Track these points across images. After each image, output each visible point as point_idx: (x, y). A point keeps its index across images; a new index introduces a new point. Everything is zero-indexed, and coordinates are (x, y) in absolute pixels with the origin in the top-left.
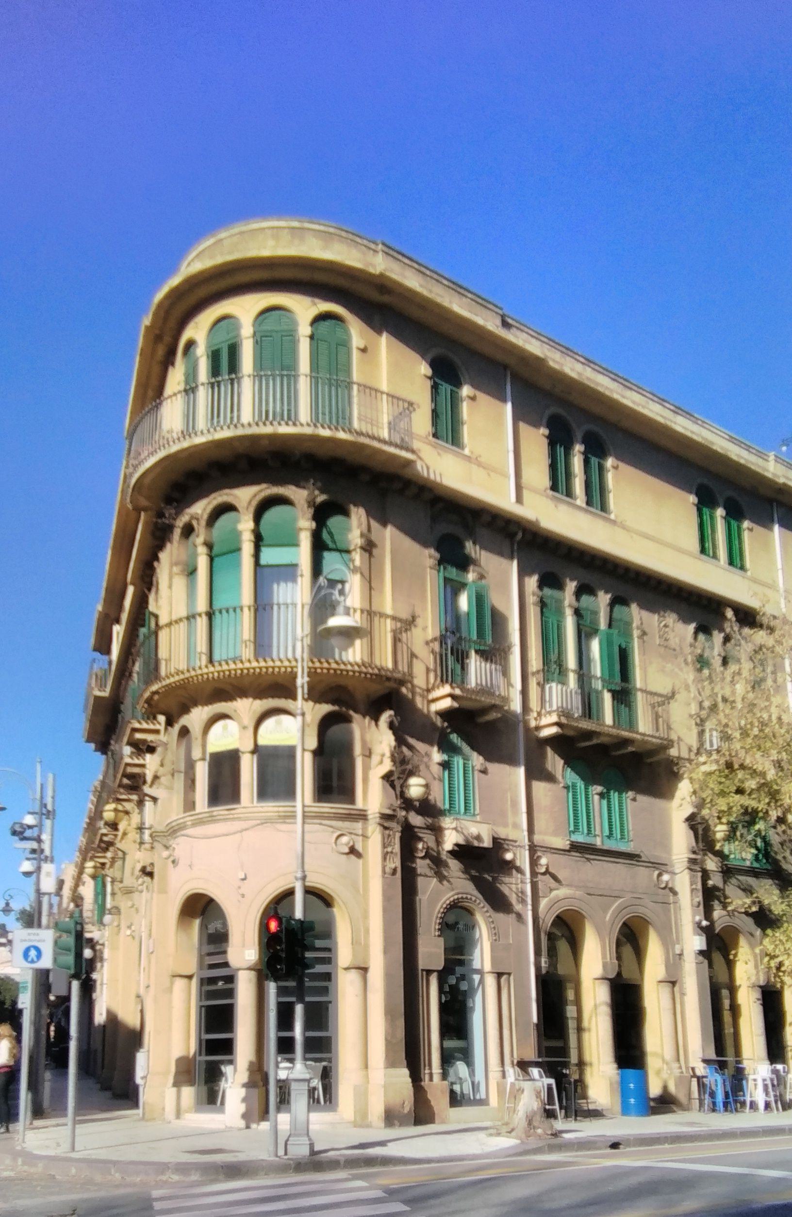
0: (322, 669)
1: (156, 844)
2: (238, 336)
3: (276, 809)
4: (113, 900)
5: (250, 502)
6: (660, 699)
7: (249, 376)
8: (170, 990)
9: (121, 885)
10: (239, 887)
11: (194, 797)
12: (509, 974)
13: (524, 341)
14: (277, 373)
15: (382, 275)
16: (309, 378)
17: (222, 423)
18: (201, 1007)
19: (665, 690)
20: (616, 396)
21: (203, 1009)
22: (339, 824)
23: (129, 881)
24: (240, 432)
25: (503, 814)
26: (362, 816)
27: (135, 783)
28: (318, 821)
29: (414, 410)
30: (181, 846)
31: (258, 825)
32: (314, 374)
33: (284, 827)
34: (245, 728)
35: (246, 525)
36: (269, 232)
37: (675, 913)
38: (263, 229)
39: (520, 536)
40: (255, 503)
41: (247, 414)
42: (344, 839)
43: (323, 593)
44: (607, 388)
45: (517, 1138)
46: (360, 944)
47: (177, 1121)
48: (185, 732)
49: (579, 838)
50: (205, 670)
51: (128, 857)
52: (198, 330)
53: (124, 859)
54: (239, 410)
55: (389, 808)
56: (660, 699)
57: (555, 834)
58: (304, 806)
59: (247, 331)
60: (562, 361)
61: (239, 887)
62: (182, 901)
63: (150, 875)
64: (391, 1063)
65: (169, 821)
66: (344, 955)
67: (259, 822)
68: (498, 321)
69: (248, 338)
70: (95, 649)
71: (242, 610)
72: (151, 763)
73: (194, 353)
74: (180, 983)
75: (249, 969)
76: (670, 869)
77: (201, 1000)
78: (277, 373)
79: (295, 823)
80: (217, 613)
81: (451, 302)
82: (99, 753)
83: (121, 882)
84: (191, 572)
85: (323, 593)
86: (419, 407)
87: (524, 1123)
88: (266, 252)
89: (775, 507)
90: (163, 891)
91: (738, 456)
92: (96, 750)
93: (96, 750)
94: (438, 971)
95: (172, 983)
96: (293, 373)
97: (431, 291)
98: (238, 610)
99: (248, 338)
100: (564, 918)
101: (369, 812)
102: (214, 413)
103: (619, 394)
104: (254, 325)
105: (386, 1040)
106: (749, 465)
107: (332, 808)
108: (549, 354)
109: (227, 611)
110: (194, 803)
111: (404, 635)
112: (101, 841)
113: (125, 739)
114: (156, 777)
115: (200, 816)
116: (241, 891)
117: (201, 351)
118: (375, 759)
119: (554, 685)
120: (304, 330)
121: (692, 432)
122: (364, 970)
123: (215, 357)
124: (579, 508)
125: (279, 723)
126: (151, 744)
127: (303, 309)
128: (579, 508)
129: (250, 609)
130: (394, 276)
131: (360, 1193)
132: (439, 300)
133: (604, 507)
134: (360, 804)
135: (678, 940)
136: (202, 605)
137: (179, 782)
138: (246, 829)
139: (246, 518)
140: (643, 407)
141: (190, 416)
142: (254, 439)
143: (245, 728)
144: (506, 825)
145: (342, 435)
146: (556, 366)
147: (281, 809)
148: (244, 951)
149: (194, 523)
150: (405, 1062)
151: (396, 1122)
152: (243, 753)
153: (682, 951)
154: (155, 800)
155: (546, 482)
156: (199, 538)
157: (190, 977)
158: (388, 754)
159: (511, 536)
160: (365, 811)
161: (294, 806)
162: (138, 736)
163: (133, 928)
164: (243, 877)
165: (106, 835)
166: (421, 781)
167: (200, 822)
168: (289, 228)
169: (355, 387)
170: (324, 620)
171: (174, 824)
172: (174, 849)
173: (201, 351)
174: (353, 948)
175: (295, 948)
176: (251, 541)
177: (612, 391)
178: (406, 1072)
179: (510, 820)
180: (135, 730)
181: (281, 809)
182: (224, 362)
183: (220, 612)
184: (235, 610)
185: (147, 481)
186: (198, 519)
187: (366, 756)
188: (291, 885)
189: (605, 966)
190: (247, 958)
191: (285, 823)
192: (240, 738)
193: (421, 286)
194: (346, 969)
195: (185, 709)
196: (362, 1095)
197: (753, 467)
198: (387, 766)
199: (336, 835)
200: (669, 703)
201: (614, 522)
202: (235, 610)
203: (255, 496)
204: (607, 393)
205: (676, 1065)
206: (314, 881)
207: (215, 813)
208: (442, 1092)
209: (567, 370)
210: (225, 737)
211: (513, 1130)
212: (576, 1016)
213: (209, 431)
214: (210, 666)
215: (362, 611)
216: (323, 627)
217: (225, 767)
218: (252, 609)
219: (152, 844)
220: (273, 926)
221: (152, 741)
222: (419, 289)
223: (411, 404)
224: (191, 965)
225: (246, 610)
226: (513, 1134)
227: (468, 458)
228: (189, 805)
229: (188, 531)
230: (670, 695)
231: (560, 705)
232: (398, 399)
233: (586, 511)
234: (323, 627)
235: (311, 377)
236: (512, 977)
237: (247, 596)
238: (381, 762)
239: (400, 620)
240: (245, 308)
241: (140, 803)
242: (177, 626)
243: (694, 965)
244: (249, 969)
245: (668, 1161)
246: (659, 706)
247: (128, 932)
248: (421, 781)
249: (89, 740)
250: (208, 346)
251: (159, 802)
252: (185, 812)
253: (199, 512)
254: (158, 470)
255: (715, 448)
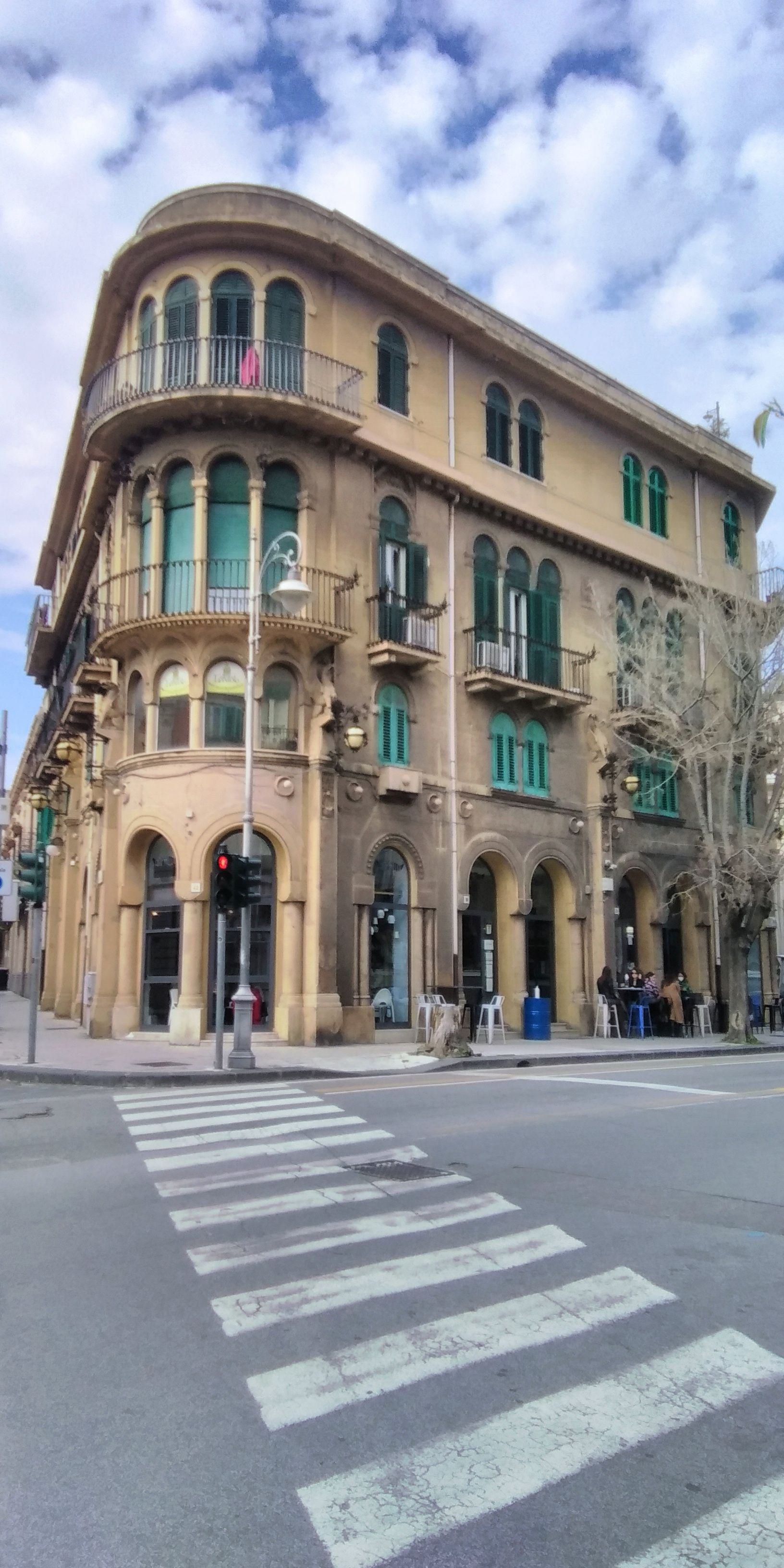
0: (269, 623)
1: (106, 782)
2: (196, 296)
3: (223, 753)
6: (581, 658)
7: (206, 339)
8: (118, 918)
9: (65, 818)
12: (434, 909)
13: (466, 311)
14: (234, 337)
16: (263, 344)
17: (179, 383)
18: (147, 934)
19: (586, 650)
20: (552, 368)
22: (282, 769)
23: (72, 814)
24: (196, 393)
26: (304, 763)
27: (83, 722)
28: (262, 766)
29: (362, 378)
30: (132, 784)
31: (206, 768)
32: (268, 341)
33: (230, 770)
34: (195, 675)
40: (209, 460)
41: (203, 378)
42: (287, 783)
43: (275, 557)
44: (543, 359)
45: (436, 1056)
46: (300, 878)
48: (136, 677)
49: (504, 786)
50: (160, 620)
51: (72, 791)
52: (156, 291)
53: (69, 792)
55: (329, 755)
56: (581, 658)
57: (481, 782)
59: (204, 292)
64: (323, 988)
65: (120, 761)
66: (284, 890)
67: (206, 765)
69: (205, 300)
72: (100, 705)
73: (153, 311)
74: (126, 914)
75: (195, 901)
76: (584, 816)
77: (147, 929)
78: (234, 337)
79: (244, 767)
80: (171, 566)
81: (399, 273)
82: (40, 687)
83: (66, 814)
84: (141, 523)
85: (275, 557)
86: (366, 375)
87: (443, 1043)
88: (225, 218)
91: (664, 428)
94: (369, 906)
95: (120, 913)
96: (248, 338)
97: (381, 262)
98: (191, 564)
99: (205, 300)
101: (310, 758)
102: (170, 371)
104: (211, 289)
105: (320, 967)
106: (674, 437)
107: (275, 754)
108: (490, 325)
109: (181, 565)
111: (347, 592)
112: (43, 773)
113: (76, 679)
114: (108, 719)
115: (151, 758)
116: (189, 829)
117: (159, 308)
118: (318, 708)
119: (484, 643)
120: (259, 295)
121: (622, 404)
122: (301, 905)
124: (514, 474)
125: (227, 672)
126: (104, 687)
128: (514, 474)
129: (202, 564)
130: (347, 247)
131: (188, 1122)
132: (388, 271)
133: (537, 474)
134: (301, 751)
135: (588, 881)
136: (153, 555)
137: (129, 725)
138: (194, 772)
140: (577, 379)
141: (145, 374)
142: (210, 400)
143: (195, 675)
144: (434, 773)
145: (293, 400)
146: (497, 338)
147: (228, 754)
148: (191, 883)
149: (150, 477)
150: (336, 988)
151: (326, 1042)
152: (193, 699)
153: (592, 890)
154: (106, 740)
155: (484, 449)
156: (153, 493)
157: (137, 907)
158: (329, 705)
159: (449, 500)
162: (89, 678)
163: (77, 858)
164: (190, 815)
165: (48, 768)
166: (360, 731)
167: (150, 763)
169: (306, 355)
170: (275, 585)
172: (124, 787)
173: (159, 308)
175: (240, 882)
176: (203, 497)
177: (548, 362)
178: (336, 996)
179: (439, 768)
180: (86, 672)
181: (228, 754)
182: (181, 322)
183: (174, 565)
184: (188, 564)
185: (104, 433)
186: (153, 473)
187: (308, 706)
189: (521, 904)
190: (193, 890)
191: (231, 766)
192: (191, 685)
193: (372, 257)
194: (286, 903)
195: (135, 653)
196: (297, 1018)
197: (677, 439)
199: (279, 778)
200: (589, 662)
201: (544, 488)
202: (188, 564)
204: (544, 364)
205: (582, 994)
206: (261, 822)
207: (165, 756)
208: (369, 1015)
209: (507, 341)
210: (177, 684)
211: (432, 1049)
212: (492, 948)
214: (163, 615)
215: (308, 569)
216: (275, 590)
217: (175, 713)
218: (205, 563)
220: (223, 862)
221: (104, 684)
222: (370, 260)
223: (359, 372)
224: (138, 896)
225: (198, 564)
228: (140, 746)
229: (143, 484)
230: (590, 654)
231: (488, 661)
232: (348, 367)
233: (520, 477)
234: (275, 590)
235: (265, 342)
237: (198, 550)
238: (322, 712)
239: (343, 579)
241: (90, 741)
242: (131, 576)
243: (602, 904)
245: (46, 923)
246: (580, 664)
247: (73, 863)
248: (360, 731)
250: (166, 307)
251: (110, 742)
252: (135, 753)
253: (154, 466)
254: (116, 424)
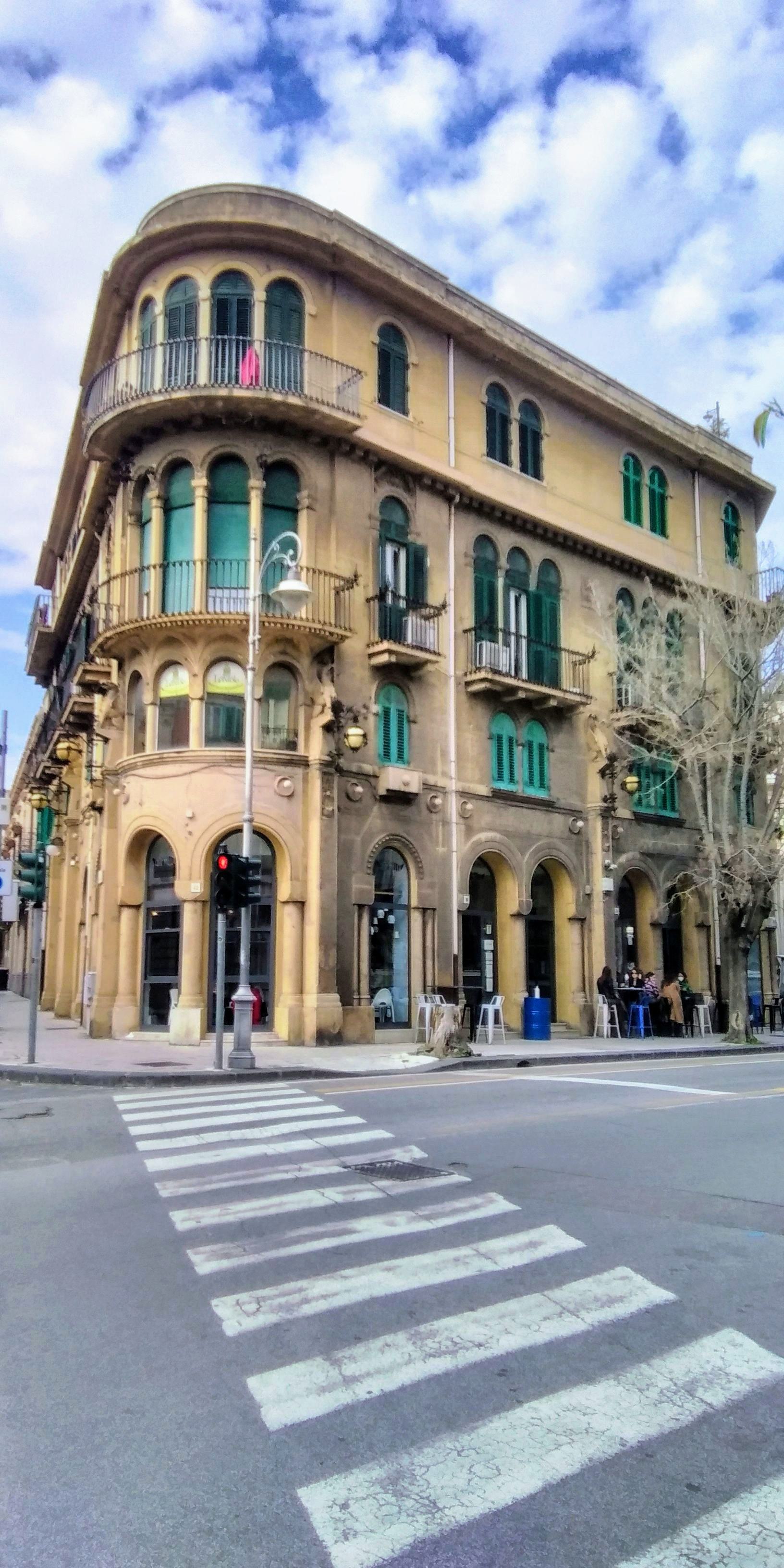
1: (106, 782)
3: (223, 753)
4: (58, 830)
5: (204, 460)
6: (581, 658)
7: (206, 339)
8: (118, 918)
9: (65, 818)
10: (187, 825)
11: (144, 737)
12: (434, 910)
15: (334, 245)
16: (263, 344)
17: (179, 383)
19: (586, 650)
21: (150, 938)
22: (282, 769)
24: (196, 393)
25: (433, 763)
26: (304, 763)
27: (83, 722)
28: (262, 766)
29: (362, 378)
30: (132, 784)
31: (206, 768)
32: (268, 341)
33: (230, 770)
34: (195, 675)
35: (199, 482)
36: (228, 197)
37: (587, 856)
38: (223, 193)
39: (457, 499)
40: (209, 460)
41: (203, 378)
42: (287, 783)
44: (543, 359)
45: (436, 1056)
46: (299, 878)
47: (566, 920)
48: (136, 677)
49: (504, 786)
50: (160, 620)
51: (72, 791)
52: (156, 290)
53: (69, 792)
54: (195, 369)
55: (328, 755)
56: (581, 658)
57: (481, 782)
58: (253, 752)
59: (204, 292)
60: (502, 332)
61: (187, 825)
62: (132, 837)
63: (100, 810)
64: (323, 988)
66: (284, 890)
67: (206, 765)
68: (443, 293)
69: (205, 300)
70: (39, 582)
71: (194, 564)
72: (100, 705)
73: (153, 311)
74: (126, 914)
77: (147, 929)
79: (244, 767)
80: (171, 566)
81: (399, 273)
82: (40, 686)
83: (66, 814)
84: (141, 523)
85: (275, 557)
87: (443, 1043)
89: (696, 475)
90: (114, 825)
92: (37, 683)
93: (37, 683)
95: (120, 913)
96: (248, 338)
97: (381, 262)
98: (191, 564)
99: (205, 300)
100: (484, 858)
101: (310, 758)
102: (170, 372)
103: (555, 366)
105: (320, 967)
108: (490, 325)
109: (181, 565)
110: (143, 745)
112: (43, 773)
113: (76, 679)
114: (108, 719)
116: (189, 829)
117: (159, 308)
118: (318, 709)
119: (484, 643)
120: (259, 295)
121: (622, 404)
122: (301, 905)
123: (171, 314)
125: (227, 672)
126: (104, 687)
127: (260, 277)
129: (202, 564)
130: (346, 247)
133: (537, 474)
134: (301, 751)
136: (153, 555)
137: (129, 724)
139: (200, 474)
140: (577, 379)
142: (210, 400)
144: (434, 773)
145: (293, 400)
146: (497, 338)
147: (228, 754)
148: (191, 884)
149: (150, 476)
151: (327, 1042)
153: (592, 890)
155: (484, 449)
156: (153, 492)
157: (138, 907)
158: (329, 705)
159: (449, 500)
160: (307, 757)
161: (538, 1020)
162: (89, 677)
163: (77, 858)
164: (190, 815)
165: (48, 768)
166: (360, 731)
168: (247, 194)
171: (125, 764)
172: (124, 787)
173: (159, 308)
174: (292, 884)
175: (240, 882)
176: (203, 497)
177: (548, 362)
178: (337, 996)
179: (439, 769)
180: (86, 672)
181: (228, 754)
183: (174, 565)
184: (188, 564)
185: (104, 433)
186: (153, 473)
188: (240, 824)
190: (193, 890)
191: (231, 766)
192: (191, 685)
193: (372, 257)
194: (285, 903)
195: (135, 653)
196: (297, 1018)
198: (328, 716)
199: (279, 778)
200: (589, 662)
202: (188, 564)
203: (209, 453)
205: (582, 994)
206: (261, 822)
207: (165, 756)
208: (369, 1015)
209: (507, 342)
210: (178, 684)
211: (432, 1049)
212: (492, 948)
213: (166, 391)
214: (163, 615)
215: (308, 569)
216: (275, 590)
217: (174, 713)
218: (205, 563)
219: (103, 781)
220: (223, 862)
225: (198, 564)
226: (432, 1053)
227: (411, 424)
228: (140, 746)
230: (590, 654)
231: (488, 661)
233: (520, 477)
234: (275, 590)
236: (436, 912)
237: (198, 550)
238: (322, 712)
239: (343, 579)
240: (203, 275)
242: (131, 576)
243: (602, 904)
244: (195, 901)
246: (580, 664)
247: (73, 863)
248: (360, 731)
249: (29, 674)
251: (110, 742)
252: (135, 753)
253: (154, 466)
254: (116, 424)
255: (642, 419)
